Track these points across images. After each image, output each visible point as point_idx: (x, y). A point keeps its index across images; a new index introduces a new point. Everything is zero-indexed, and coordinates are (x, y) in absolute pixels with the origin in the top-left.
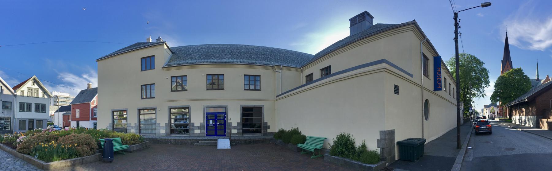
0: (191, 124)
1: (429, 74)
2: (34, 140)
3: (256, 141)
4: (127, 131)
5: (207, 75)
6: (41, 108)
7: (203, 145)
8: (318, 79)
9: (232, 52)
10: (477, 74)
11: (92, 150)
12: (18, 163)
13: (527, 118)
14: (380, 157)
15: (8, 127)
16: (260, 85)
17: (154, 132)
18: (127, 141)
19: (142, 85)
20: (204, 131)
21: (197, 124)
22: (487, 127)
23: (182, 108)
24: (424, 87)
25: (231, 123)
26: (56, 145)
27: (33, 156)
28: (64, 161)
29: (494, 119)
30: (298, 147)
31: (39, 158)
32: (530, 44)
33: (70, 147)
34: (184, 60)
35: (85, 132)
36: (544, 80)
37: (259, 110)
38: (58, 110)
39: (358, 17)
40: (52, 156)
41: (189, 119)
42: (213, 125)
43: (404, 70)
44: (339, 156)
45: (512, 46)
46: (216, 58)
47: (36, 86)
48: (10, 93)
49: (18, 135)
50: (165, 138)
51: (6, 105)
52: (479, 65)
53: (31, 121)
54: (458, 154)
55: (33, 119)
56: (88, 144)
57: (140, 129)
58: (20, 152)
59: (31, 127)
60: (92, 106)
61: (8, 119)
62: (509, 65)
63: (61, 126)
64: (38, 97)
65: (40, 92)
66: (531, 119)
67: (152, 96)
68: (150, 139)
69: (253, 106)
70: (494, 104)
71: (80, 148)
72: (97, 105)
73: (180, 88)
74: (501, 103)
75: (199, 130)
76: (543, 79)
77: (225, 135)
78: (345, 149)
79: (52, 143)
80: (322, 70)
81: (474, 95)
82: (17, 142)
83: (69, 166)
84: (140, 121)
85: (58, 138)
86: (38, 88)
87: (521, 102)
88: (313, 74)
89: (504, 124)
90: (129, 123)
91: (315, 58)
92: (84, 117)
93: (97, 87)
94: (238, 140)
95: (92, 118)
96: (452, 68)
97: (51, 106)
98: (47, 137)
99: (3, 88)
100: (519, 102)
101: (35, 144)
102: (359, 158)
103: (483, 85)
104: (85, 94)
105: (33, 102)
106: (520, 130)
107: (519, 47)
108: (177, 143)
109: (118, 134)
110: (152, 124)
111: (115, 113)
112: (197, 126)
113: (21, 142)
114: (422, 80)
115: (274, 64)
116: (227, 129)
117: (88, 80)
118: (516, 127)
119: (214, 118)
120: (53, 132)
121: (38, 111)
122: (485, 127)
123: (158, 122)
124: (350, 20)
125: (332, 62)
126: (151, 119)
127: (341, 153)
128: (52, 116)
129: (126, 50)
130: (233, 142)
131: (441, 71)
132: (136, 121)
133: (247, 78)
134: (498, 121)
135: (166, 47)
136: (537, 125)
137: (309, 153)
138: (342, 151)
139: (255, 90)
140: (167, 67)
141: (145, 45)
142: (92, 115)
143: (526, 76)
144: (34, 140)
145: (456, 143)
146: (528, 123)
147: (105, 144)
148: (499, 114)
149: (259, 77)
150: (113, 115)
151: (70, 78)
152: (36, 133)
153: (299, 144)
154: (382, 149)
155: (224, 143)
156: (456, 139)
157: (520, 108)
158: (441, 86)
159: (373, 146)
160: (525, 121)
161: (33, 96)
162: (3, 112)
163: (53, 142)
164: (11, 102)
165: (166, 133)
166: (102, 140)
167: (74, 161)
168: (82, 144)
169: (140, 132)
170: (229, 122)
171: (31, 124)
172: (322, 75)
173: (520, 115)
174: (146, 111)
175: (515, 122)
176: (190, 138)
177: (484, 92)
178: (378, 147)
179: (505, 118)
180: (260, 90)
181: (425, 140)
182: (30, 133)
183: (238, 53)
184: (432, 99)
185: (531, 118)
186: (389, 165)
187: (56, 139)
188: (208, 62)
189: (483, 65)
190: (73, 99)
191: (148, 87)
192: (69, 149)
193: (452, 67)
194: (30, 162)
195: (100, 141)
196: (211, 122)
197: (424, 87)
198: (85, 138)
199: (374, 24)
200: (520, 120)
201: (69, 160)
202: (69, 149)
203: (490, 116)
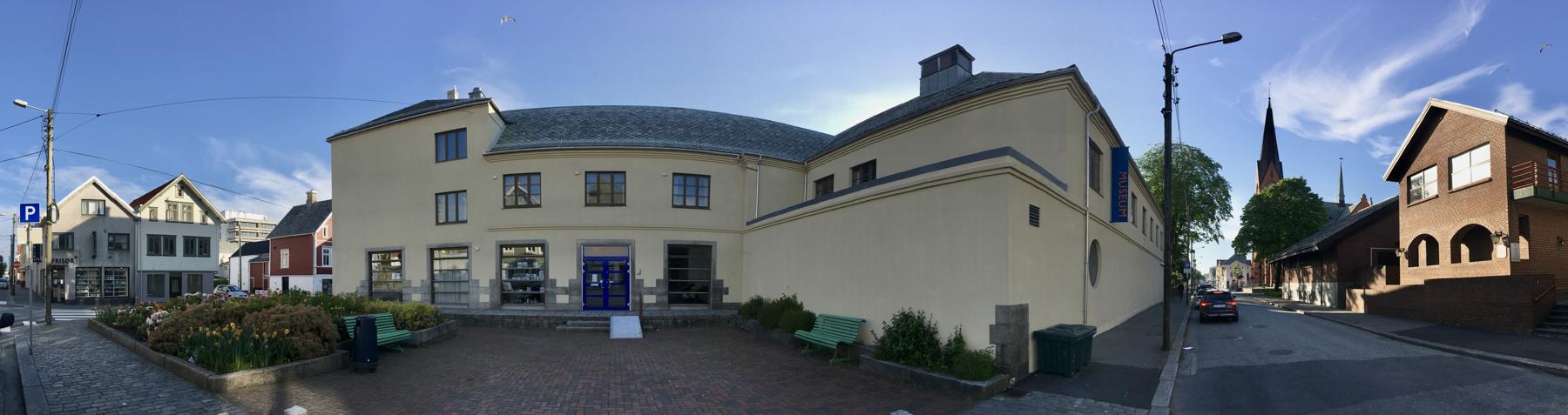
0: (549, 283)
1: (1100, 186)
2: (186, 321)
3: (696, 322)
4: (404, 298)
5: (586, 172)
6: (199, 246)
7: (577, 331)
8: (844, 190)
9: (643, 123)
10: (1203, 189)
11: (327, 344)
12: (153, 375)
13: (1317, 287)
14: (995, 364)
15: (122, 290)
16: (709, 197)
17: (464, 299)
18: (406, 320)
19: (437, 195)
20: (579, 299)
21: (562, 282)
22: (1229, 307)
23: (524, 246)
24: (1090, 213)
25: (642, 280)
26: (239, 332)
27: (185, 357)
28: (260, 371)
29: (1241, 290)
30: (796, 338)
31: (200, 362)
32: (1325, 127)
33: (273, 336)
34: (534, 139)
35: (305, 300)
36: (1356, 204)
37: (704, 252)
38: (238, 252)
39: (939, 59)
40: (232, 360)
41: (545, 268)
42: (600, 284)
43: (1050, 175)
44: (898, 361)
45: (1289, 134)
46: (607, 135)
47: (187, 198)
48: (124, 215)
49: (147, 308)
50: (491, 314)
51: (117, 241)
52: (1209, 171)
53: (176, 277)
54: (1165, 362)
55: (180, 273)
56: (317, 330)
57: (433, 294)
58: (157, 350)
59: (175, 290)
60: (317, 243)
61: (122, 273)
62: (1275, 172)
63: (246, 287)
64: (193, 223)
65: (197, 211)
66: (1327, 290)
67: (460, 219)
68: (455, 317)
69: (692, 243)
70: (1239, 257)
71: (297, 338)
72: (331, 240)
73: (522, 202)
74: (1255, 254)
75: (568, 296)
76: (1353, 200)
77: (627, 308)
78: (914, 345)
79: (230, 328)
80: (855, 169)
81: (1195, 236)
82: (148, 326)
83: (271, 383)
84: (432, 276)
85: (243, 315)
86: (192, 201)
87: (1303, 252)
88: (832, 176)
89: (1264, 300)
90: (407, 279)
91: (838, 142)
92: (300, 267)
93: (330, 198)
94: (658, 318)
95: (318, 269)
96: (1148, 174)
97: (223, 243)
98: (217, 313)
99: (109, 203)
100: (1298, 253)
101: (189, 330)
102: (950, 368)
103: (1217, 215)
104: (301, 214)
105: (180, 234)
106: (1303, 313)
107: (1299, 134)
108: (515, 324)
109: (385, 304)
110: (460, 282)
111: (374, 257)
112: (563, 288)
113: (157, 324)
114: (1086, 196)
115: (743, 151)
116: (634, 294)
117: (306, 185)
118: (1292, 306)
119: (601, 269)
120: (231, 302)
121: (192, 252)
122: (1224, 306)
123: (474, 277)
124: (921, 63)
125: (888, 155)
126: (454, 271)
127: (904, 356)
128: (225, 266)
129: (399, 116)
130: (647, 324)
131: (1127, 180)
132: (425, 276)
133: (679, 180)
134: (1250, 295)
135: (491, 111)
136: (1341, 302)
137: (823, 352)
138: (908, 350)
139: (697, 207)
140: (494, 153)
141: (443, 105)
142: (319, 263)
143: (1316, 196)
144: (186, 321)
145: (1161, 338)
146: (1318, 297)
147: (358, 328)
148: (1252, 278)
149: (706, 180)
150: (370, 262)
151: (265, 179)
152: (191, 303)
153: (800, 331)
154: (999, 349)
155: (625, 326)
156: (1161, 330)
157: (1302, 266)
158: (1126, 212)
159: (979, 340)
160: (1313, 294)
161: (179, 220)
162: (110, 258)
163: (232, 324)
164: (128, 235)
165: (492, 303)
166: (350, 320)
167: (283, 370)
168: (302, 331)
169: (433, 301)
170: (637, 277)
171: (175, 282)
172: (854, 180)
173: (1300, 280)
174: (443, 252)
175: (1290, 297)
176: (546, 314)
177: (1218, 229)
178: (991, 343)
179: (1266, 288)
180: (708, 208)
181: (1095, 329)
182: (175, 304)
183: (658, 125)
184: (1108, 241)
185: (1326, 287)
186: (1017, 383)
187: (238, 318)
188: (588, 144)
189: (1217, 170)
190: (274, 227)
191: (452, 198)
192: (271, 340)
193: (1148, 172)
194: (177, 372)
195: (343, 321)
196: (595, 277)
197: (1090, 213)
198: (309, 316)
199: (975, 72)
200: (1302, 292)
201: (272, 369)
202: (271, 340)
203: (1230, 283)
